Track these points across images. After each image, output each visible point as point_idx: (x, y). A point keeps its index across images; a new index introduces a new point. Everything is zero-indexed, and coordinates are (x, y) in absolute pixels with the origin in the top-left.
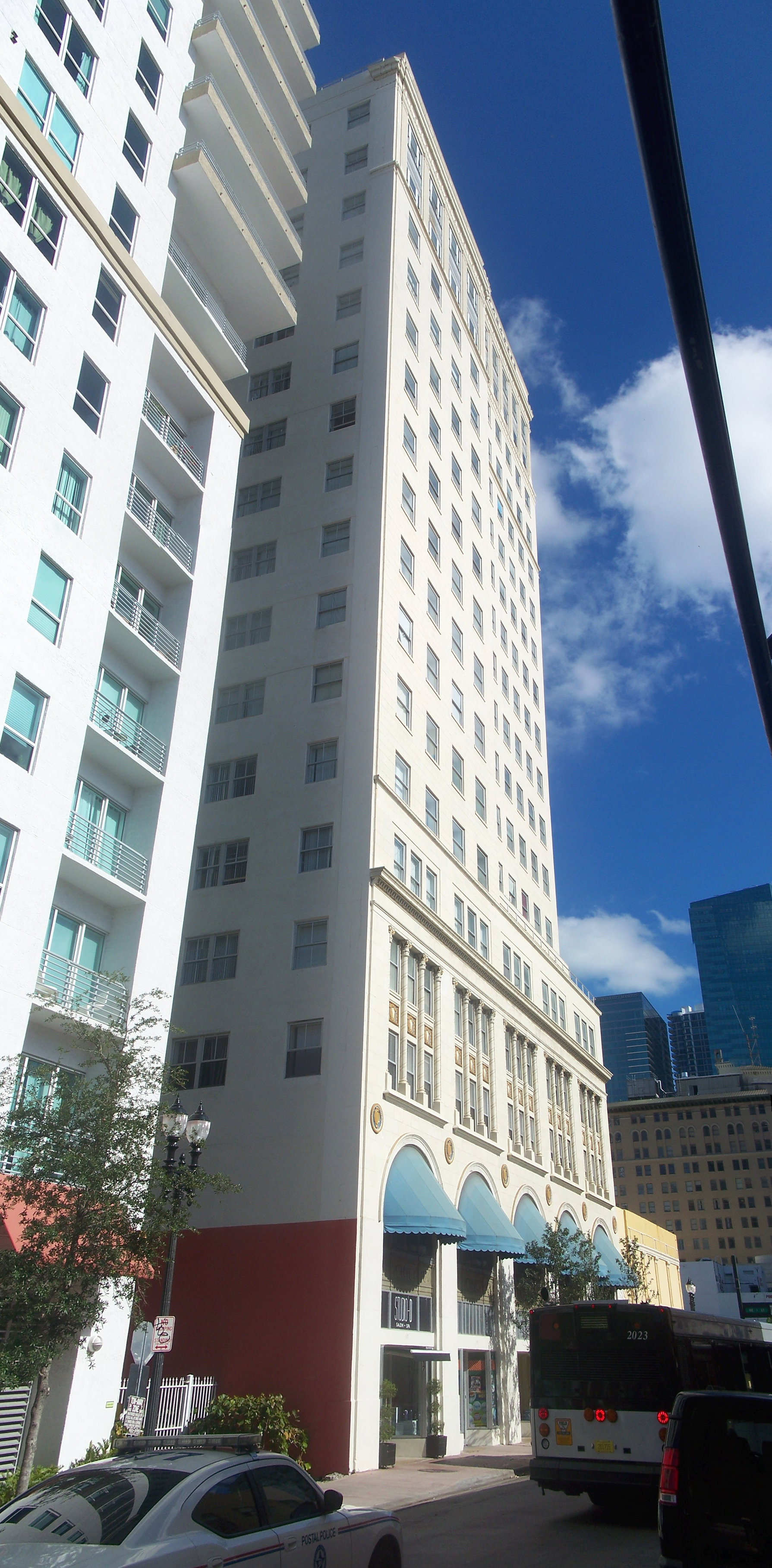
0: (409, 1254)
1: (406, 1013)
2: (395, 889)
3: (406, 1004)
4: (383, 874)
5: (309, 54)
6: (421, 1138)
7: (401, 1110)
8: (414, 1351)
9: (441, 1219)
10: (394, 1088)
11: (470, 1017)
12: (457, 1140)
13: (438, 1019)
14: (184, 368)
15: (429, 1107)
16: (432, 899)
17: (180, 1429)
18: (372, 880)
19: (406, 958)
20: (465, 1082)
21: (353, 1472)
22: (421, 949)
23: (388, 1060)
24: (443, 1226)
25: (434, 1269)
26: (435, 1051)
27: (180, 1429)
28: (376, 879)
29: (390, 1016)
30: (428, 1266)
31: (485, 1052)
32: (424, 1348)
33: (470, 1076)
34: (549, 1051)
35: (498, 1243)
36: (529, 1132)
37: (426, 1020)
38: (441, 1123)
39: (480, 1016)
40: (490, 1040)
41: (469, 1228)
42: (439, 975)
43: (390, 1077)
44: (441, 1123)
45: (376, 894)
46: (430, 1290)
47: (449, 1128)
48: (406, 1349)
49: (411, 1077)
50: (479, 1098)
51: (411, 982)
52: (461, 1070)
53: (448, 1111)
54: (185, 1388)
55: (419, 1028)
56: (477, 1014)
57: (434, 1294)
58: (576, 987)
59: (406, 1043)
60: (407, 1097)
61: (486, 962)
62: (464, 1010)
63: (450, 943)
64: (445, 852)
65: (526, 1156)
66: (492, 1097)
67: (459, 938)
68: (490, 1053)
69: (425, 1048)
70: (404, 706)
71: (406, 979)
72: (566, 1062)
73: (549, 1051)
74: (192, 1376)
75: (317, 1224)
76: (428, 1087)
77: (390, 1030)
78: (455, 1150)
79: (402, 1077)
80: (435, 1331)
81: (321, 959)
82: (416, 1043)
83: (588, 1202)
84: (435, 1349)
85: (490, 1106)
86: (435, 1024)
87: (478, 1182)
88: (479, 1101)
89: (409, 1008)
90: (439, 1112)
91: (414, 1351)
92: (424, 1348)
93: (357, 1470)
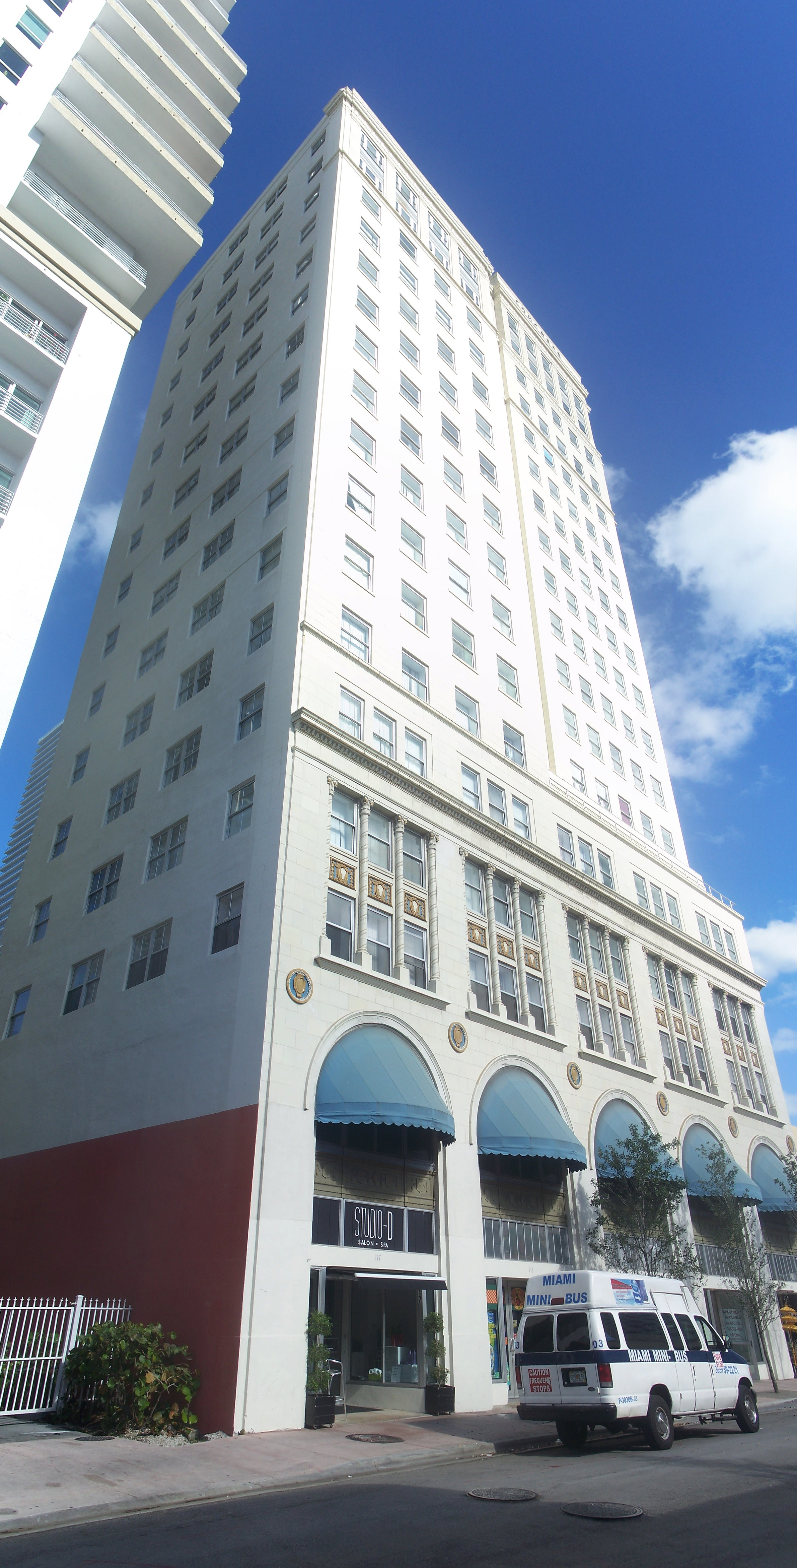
0: (375, 1155)
1: (593, 979)
2: (357, 751)
3: (593, 970)
4: (303, 716)
5: (226, 36)
6: (395, 1017)
7: (765, 1124)
8: (358, 1275)
9: (544, 1141)
10: (673, 1078)
11: (731, 1013)
12: (670, 1094)
13: (545, 942)
14: (41, 268)
15: (708, 1091)
16: (733, 953)
17: (59, 1361)
18: (294, 724)
19: (587, 931)
20: (737, 1068)
21: (242, 1433)
22: (674, 960)
23: (579, 1021)
24: (423, 1117)
25: (435, 1175)
26: (763, 1070)
27: (59, 1361)
28: (298, 724)
29: (658, 1019)
30: (558, 1193)
31: (750, 1040)
32: (419, 1274)
33: (741, 1063)
34: (567, 902)
35: (533, 1146)
36: (679, 1054)
37: (750, 1048)
38: (721, 1104)
39: (517, 895)
40: (754, 1030)
41: (763, 1192)
42: (626, 944)
43: (668, 1070)
44: (650, 1079)
45: (298, 739)
46: (431, 1203)
47: (729, 1108)
48: (350, 1272)
49: (749, 1092)
50: (738, 1074)
51: (596, 953)
52: (731, 1059)
53: (725, 1092)
54: (68, 1311)
55: (668, 1019)
56: (723, 1002)
57: (436, 1208)
58: (711, 895)
59: (402, 923)
60: (686, 1085)
61: (531, 845)
62: (724, 1007)
63: (538, 858)
64: (495, 755)
65: (635, 1063)
66: (707, 1055)
67: (722, 957)
68: (756, 1042)
69: (755, 1069)
70: (362, 570)
71: (683, 996)
72: (683, 961)
73: (711, 979)
74: (80, 1298)
75: (224, 1114)
76: (703, 1075)
77: (470, 949)
78: (669, 1102)
79: (359, 946)
80: (438, 1253)
81: (247, 823)
82: (489, 954)
83: (737, 1117)
84: (439, 1275)
85: (765, 1086)
86: (758, 1049)
87: (700, 1132)
88: (521, 988)
89: (596, 975)
90: (435, 992)
91: (358, 1275)
92: (419, 1274)
93: (246, 1431)
